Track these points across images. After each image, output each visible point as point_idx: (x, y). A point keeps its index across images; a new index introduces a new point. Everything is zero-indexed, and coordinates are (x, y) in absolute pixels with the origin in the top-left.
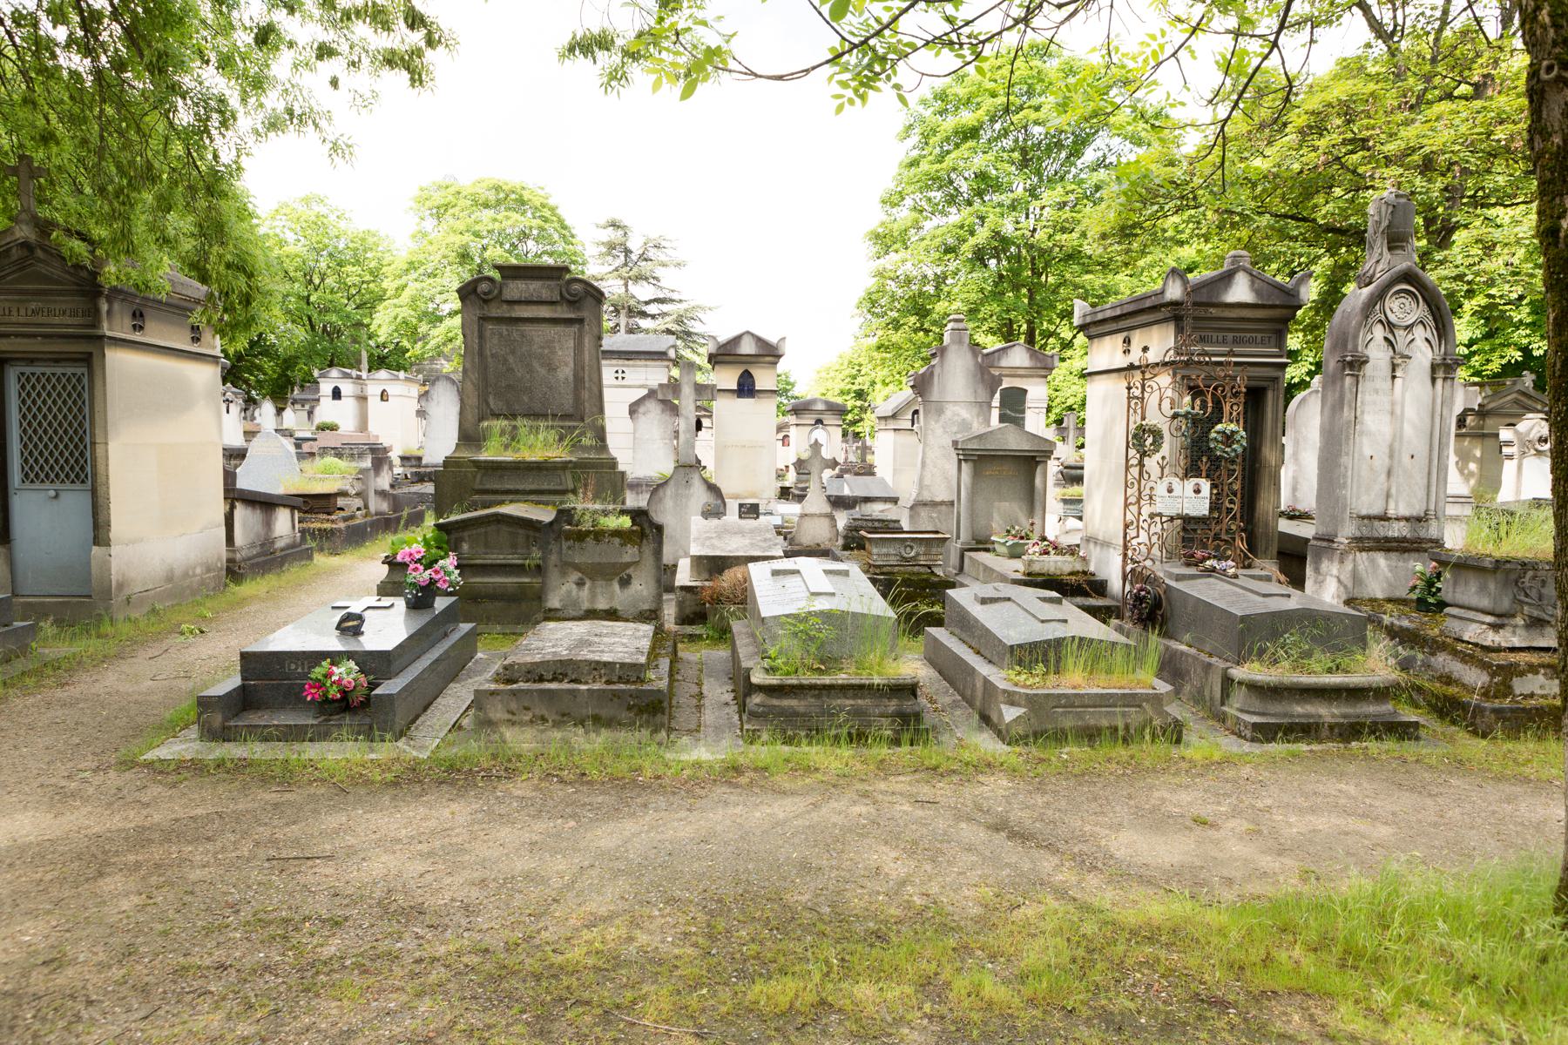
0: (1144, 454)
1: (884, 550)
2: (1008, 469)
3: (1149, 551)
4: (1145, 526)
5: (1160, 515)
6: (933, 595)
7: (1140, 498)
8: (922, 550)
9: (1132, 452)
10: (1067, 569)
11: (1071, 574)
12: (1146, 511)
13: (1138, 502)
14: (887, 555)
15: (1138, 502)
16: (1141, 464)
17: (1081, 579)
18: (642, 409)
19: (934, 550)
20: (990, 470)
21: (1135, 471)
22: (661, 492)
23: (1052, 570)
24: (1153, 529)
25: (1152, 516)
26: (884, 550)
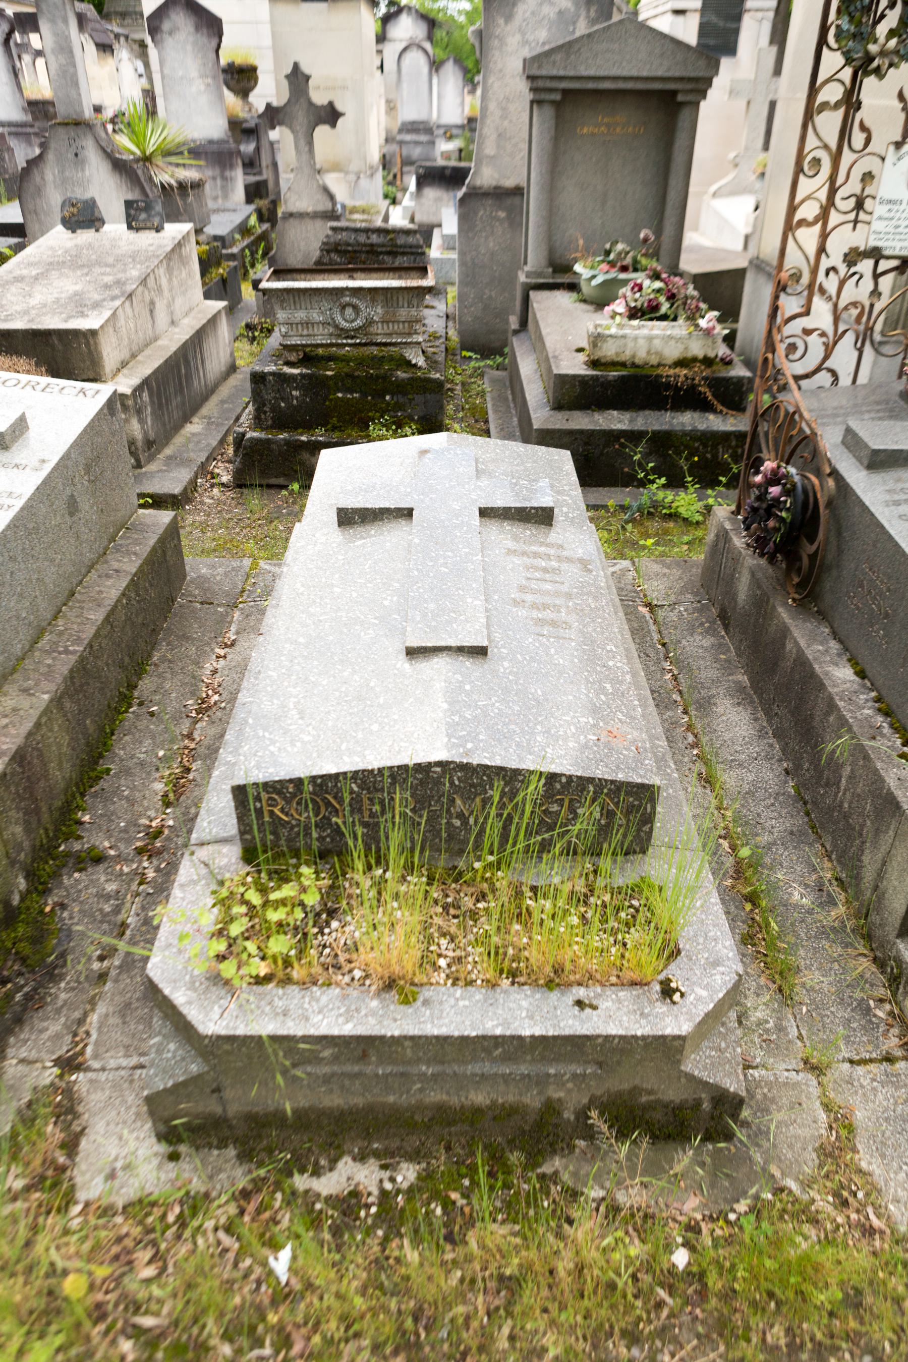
0: (864, 67)
1: (301, 315)
2: (623, 123)
3: (829, 351)
4: (831, 285)
5: (876, 254)
6: (398, 407)
7: (830, 203)
8: (378, 312)
9: (832, 60)
10: (673, 353)
11: (682, 363)
12: (838, 245)
13: (824, 216)
14: (307, 324)
15: (824, 216)
16: (851, 102)
17: (699, 373)
18: (166, 26)
19: (403, 313)
20: (592, 125)
21: (829, 124)
22: (36, 175)
23: (641, 355)
24: (850, 293)
25: (852, 257)
26: (301, 315)
